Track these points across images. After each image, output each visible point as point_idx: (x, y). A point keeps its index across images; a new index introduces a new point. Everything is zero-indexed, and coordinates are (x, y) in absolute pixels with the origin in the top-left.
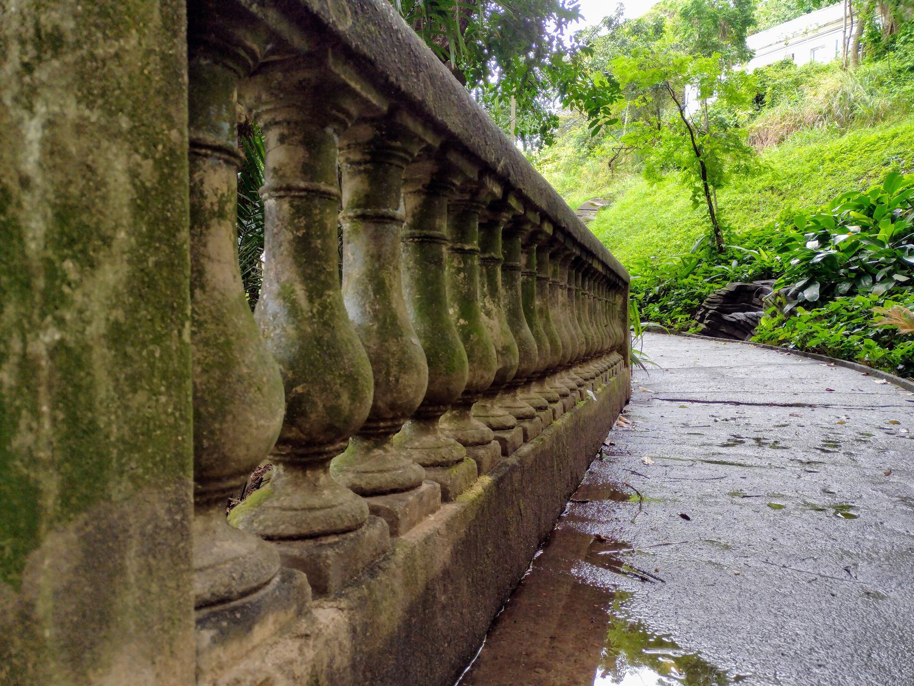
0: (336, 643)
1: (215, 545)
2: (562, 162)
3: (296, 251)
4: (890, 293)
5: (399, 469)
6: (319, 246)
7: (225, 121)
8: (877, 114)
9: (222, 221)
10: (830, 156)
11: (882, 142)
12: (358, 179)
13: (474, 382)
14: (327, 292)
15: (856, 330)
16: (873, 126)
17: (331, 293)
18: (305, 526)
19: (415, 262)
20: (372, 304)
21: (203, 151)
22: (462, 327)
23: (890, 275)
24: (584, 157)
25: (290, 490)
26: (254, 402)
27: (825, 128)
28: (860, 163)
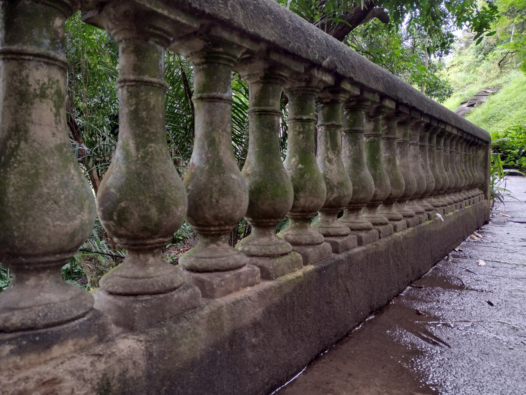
0: (130, 362)
1: (39, 295)
2: (464, 65)
3: (130, 120)
5: (223, 257)
6: (145, 116)
7: (46, 38)
9: (44, 100)
12: (199, 74)
13: (307, 205)
14: (150, 145)
17: (153, 145)
18: (128, 288)
19: (256, 128)
20: (206, 153)
21: (27, 57)
22: (301, 169)
24: (480, 61)
25: (130, 266)
26: (51, 210)
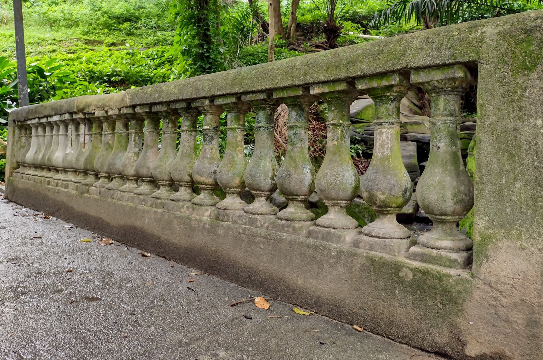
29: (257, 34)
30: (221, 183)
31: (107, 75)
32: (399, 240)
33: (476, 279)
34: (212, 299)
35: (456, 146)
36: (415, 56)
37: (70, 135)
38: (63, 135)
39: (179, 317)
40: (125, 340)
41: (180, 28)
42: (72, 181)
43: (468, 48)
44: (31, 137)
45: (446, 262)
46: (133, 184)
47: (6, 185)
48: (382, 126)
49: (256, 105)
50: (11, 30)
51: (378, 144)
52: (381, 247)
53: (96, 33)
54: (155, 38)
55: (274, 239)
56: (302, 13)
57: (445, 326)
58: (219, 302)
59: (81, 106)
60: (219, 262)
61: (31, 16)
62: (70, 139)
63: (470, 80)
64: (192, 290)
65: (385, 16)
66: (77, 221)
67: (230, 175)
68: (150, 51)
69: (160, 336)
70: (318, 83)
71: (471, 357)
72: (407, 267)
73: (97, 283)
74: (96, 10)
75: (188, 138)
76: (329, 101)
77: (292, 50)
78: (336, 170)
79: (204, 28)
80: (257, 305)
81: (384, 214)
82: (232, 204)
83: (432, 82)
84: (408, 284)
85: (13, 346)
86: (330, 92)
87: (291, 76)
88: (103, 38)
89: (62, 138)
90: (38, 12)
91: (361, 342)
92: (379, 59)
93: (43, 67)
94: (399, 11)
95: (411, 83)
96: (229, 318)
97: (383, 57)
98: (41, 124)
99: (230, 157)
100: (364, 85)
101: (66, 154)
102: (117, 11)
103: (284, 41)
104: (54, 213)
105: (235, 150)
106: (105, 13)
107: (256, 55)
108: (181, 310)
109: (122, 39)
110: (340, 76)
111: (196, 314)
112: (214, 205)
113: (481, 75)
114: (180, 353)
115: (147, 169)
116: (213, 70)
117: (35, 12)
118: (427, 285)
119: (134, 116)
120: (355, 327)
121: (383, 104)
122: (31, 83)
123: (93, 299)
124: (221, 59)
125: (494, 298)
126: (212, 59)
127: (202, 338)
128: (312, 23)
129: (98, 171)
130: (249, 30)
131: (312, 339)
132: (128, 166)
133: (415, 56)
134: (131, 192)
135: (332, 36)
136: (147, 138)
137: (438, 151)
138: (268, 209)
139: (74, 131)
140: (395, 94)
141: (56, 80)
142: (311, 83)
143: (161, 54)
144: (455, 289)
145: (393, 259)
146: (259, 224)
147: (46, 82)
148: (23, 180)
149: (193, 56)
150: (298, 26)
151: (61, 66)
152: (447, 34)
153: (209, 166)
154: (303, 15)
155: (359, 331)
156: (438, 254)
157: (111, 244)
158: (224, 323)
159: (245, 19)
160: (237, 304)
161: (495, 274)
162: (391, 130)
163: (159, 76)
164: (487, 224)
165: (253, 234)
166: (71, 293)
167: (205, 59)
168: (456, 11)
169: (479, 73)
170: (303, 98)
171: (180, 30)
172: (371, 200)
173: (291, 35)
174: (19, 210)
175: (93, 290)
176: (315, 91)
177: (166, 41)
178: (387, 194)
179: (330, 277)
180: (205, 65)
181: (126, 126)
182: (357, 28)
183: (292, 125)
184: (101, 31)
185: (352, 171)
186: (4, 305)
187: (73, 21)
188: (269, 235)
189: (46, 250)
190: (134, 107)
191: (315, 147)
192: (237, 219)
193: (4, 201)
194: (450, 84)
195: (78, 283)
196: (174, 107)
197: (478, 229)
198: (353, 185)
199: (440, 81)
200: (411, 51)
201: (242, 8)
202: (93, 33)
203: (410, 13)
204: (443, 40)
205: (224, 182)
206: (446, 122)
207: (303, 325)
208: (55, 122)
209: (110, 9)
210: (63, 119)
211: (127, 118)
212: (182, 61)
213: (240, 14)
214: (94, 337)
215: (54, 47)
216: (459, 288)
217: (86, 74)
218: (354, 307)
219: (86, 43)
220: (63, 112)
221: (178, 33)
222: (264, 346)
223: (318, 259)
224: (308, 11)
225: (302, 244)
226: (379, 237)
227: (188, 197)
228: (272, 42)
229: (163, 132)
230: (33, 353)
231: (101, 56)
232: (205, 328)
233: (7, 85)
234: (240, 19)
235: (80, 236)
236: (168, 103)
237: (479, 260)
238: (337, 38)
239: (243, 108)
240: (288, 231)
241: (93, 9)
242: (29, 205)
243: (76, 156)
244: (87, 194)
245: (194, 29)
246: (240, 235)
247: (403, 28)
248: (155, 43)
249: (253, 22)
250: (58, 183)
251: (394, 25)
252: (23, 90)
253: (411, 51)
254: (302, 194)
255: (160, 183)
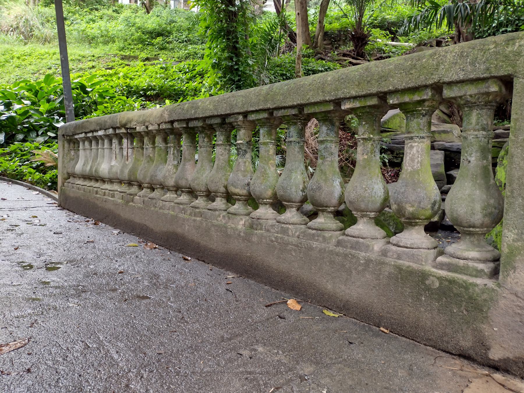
4: (46, 142)
8: (46, 38)
10: (17, 56)
11: (47, 55)
15: (26, 163)
16: (44, 44)
23: (47, 131)
27: (15, 37)
28: (35, 64)
29: (284, 44)
30: (254, 194)
31: (143, 90)
32: (426, 250)
33: (502, 289)
34: (249, 300)
35: (487, 160)
36: (448, 70)
37: (114, 149)
38: (107, 148)
39: (220, 315)
40: (174, 335)
41: (210, 41)
42: (117, 191)
43: (503, 61)
44: (79, 150)
45: (473, 272)
46: (173, 194)
47: (59, 194)
48: (413, 140)
49: (288, 120)
50: (54, 48)
51: (408, 158)
52: (409, 256)
53: (131, 49)
54: (186, 51)
55: (305, 247)
56: (329, 22)
57: (469, 332)
58: (255, 302)
59: (124, 122)
60: (253, 267)
61: (71, 34)
62: (114, 152)
63: (504, 93)
64: (230, 291)
65: (415, 22)
66: (123, 227)
67: (263, 187)
68: (182, 65)
69: (204, 332)
70: (349, 98)
71: (494, 360)
72: (433, 276)
73: (146, 283)
74: (130, 26)
75: (223, 152)
76: (360, 116)
77: (319, 59)
78: (365, 183)
79: (234, 40)
80: (289, 306)
81: (412, 225)
82: (264, 214)
83: (465, 96)
84: (434, 291)
85: (80, 336)
86: (361, 107)
87: (323, 92)
88: (137, 53)
89: (107, 151)
90: (77, 30)
91: (387, 343)
92: (412, 74)
93: (86, 84)
94: (430, 16)
95: (443, 97)
96: (264, 318)
97: (415, 72)
98: (87, 138)
99: (263, 170)
100: (395, 99)
101: (111, 166)
102: (150, 26)
103: (311, 51)
104: (102, 220)
105: (268, 163)
106: (139, 28)
107: (284, 65)
108: (221, 309)
109: (155, 53)
110: (372, 91)
111: (235, 313)
112: (248, 214)
113: (517, 89)
114: (223, 347)
115: (186, 181)
116: (242, 82)
117: (75, 30)
118: (453, 293)
119: (172, 131)
120: (382, 329)
121: (415, 118)
122: (75, 99)
123: (144, 298)
124: (250, 71)
125: (519, 307)
126: (241, 71)
127: (241, 334)
128: (339, 31)
129: (141, 181)
130: (277, 41)
131: (341, 339)
132: (168, 178)
133: (448, 70)
134: (172, 202)
135: (360, 44)
136: (185, 152)
137: (469, 165)
138: (299, 219)
139: (118, 145)
140: (427, 109)
141: (97, 96)
142: (342, 98)
143: (193, 67)
144: (481, 297)
145: (421, 268)
146: (290, 233)
147: (88, 98)
148: (74, 190)
149: (223, 69)
150: (326, 34)
151: (101, 81)
152: (482, 47)
153: (243, 178)
154: (331, 23)
155: (385, 333)
156: (465, 264)
157: (155, 248)
158: (261, 322)
159: (272, 30)
160: (271, 305)
161: (521, 285)
162: (421, 144)
163: (191, 90)
164: (516, 236)
165: (285, 242)
166: (124, 292)
167: (234, 72)
168: (491, 15)
169: (514, 87)
170: (334, 113)
171: (210, 44)
172: (400, 211)
173: (319, 45)
174: (72, 217)
175: (143, 290)
176: (346, 106)
177: (197, 54)
178: (415, 206)
179: (358, 283)
180: (235, 77)
181: (165, 141)
182: (385, 35)
183: (323, 139)
184: (135, 47)
185: (381, 184)
186: (69, 301)
187: (109, 37)
188: (300, 243)
189: (99, 253)
190: (172, 122)
191: (342, 157)
192: (270, 228)
193: (58, 208)
194: (483, 99)
195: (129, 283)
196: (209, 123)
197: (506, 241)
198: (382, 197)
199: (473, 96)
200: (445, 66)
201: (270, 18)
202: (128, 48)
203: (441, 19)
204: (478, 54)
205: (257, 193)
206: (478, 136)
207: (333, 325)
208: (100, 136)
209: (143, 25)
210: (108, 134)
211: (166, 133)
212: (213, 74)
213: (267, 24)
214: (148, 331)
215: (94, 64)
216: (485, 296)
217: (124, 89)
218: (381, 311)
219: (122, 59)
220: (107, 127)
221: (208, 46)
222: (297, 343)
223: (347, 266)
224: (336, 19)
225: (331, 252)
226: (407, 248)
227: (223, 207)
228: (299, 52)
229: (200, 145)
230: (97, 343)
231: (137, 71)
232: (244, 326)
233: (54, 101)
234: (267, 30)
235: (127, 240)
236: (204, 119)
237: (506, 271)
238: (365, 46)
239: (275, 123)
240: (318, 240)
241: (127, 25)
242: (80, 212)
243: (120, 168)
244: (132, 203)
245: (224, 42)
246: (272, 242)
247: (433, 34)
248: (187, 57)
249: (280, 32)
250: (105, 192)
251: (424, 30)
252: (69, 106)
253: (445, 66)
254: (332, 206)
255: (198, 193)
